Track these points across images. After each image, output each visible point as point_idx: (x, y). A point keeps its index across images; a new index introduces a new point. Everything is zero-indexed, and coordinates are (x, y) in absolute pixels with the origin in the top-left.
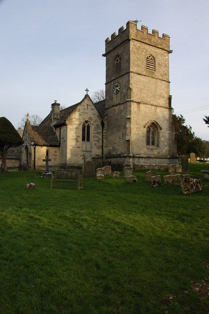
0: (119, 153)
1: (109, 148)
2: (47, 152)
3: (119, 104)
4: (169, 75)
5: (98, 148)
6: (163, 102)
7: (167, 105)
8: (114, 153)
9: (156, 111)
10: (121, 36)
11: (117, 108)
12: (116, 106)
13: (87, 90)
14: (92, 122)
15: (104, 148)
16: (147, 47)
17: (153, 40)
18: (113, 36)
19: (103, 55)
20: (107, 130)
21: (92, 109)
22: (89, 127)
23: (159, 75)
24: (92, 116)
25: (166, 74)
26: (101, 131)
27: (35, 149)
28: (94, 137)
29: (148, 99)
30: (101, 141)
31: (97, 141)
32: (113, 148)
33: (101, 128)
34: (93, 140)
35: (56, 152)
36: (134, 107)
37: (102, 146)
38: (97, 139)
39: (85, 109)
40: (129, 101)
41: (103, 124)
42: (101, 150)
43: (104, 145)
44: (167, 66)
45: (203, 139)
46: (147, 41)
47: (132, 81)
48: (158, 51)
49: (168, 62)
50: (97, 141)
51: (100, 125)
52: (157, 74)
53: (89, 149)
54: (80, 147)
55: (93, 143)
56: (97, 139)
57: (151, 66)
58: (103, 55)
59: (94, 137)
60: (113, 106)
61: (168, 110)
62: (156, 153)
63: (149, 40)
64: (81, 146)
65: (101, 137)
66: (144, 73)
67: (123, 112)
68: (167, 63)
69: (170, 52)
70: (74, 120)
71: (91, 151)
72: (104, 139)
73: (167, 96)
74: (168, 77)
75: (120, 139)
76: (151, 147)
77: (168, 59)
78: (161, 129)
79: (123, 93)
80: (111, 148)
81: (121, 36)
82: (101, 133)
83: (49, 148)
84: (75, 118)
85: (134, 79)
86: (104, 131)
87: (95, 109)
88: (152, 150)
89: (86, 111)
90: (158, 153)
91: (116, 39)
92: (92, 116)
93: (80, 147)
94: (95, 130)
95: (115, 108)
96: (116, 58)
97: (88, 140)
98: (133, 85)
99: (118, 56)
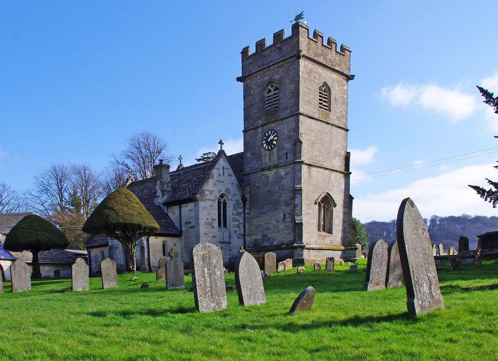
0: (275, 243)
1: (254, 237)
2: (164, 245)
3: (276, 167)
4: (347, 118)
5: (238, 238)
6: (339, 164)
7: (342, 169)
8: (266, 244)
9: (329, 177)
10: (280, 49)
11: (271, 174)
12: (269, 169)
13: (221, 143)
14: (230, 197)
15: (248, 239)
16: (320, 70)
17: (330, 56)
18: (260, 44)
19: (239, 79)
20: (250, 210)
21: (229, 175)
22: (225, 204)
23: (335, 118)
24: (230, 187)
25: (343, 117)
26: (241, 210)
27: (148, 240)
28: (233, 221)
29: (321, 159)
30: (242, 226)
31: (238, 226)
32: (264, 236)
33: (241, 206)
34: (232, 226)
35: (175, 245)
36: (304, 168)
37: (244, 235)
38: (237, 223)
39: (220, 175)
40: (299, 162)
41: (244, 200)
42: (243, 240)
43: (246, 233)
44: (345, 103)
45: (456, 216)
46: (321, 60)
47: (302, 130)
48: (335, 76)
49: (347, 96)
50: (238, 226)
51: (241, 202)
52: (333, 118)
53: (227, 240)
54: (216, 237)
55: (233, 229)
56: (237, 223)
57: (325, 104)
58: (239, 79)
59: (233, 221)
60: (263, 170)
61: (342, 175)
62: (329, 242)
63: (324, 57)
64: (217, 234)
65: (242, 221)
66: (317, 117)
67: (284, 181)
68: (345, 96)
69: (350, 78)
70: (207, 193)
71: (230, 243)
72: (246, 224)
73: (343, 154)
74: (346, 121)
75: (278, 221)
76: (323, 233)
77: (347, 90)
78: (335, 206)
79: (283, 148)
80: (259, 237)
81: (280, 49)
82: (241, 213)
83: (164, 239)
84: (208, 190)
85: (306, 127)
86: (247, 211)
87: (233, 175)
88: (324, 238)
89: (222, 178)
90: (331, 242)
91: (267, 53)
92: (230, 187)
93: (216, 237)
94: (234, 209)
95: (267, 173)
96: (267, 86)
97: (225, 226)
98: (303, 136)
99: (270, 82)
